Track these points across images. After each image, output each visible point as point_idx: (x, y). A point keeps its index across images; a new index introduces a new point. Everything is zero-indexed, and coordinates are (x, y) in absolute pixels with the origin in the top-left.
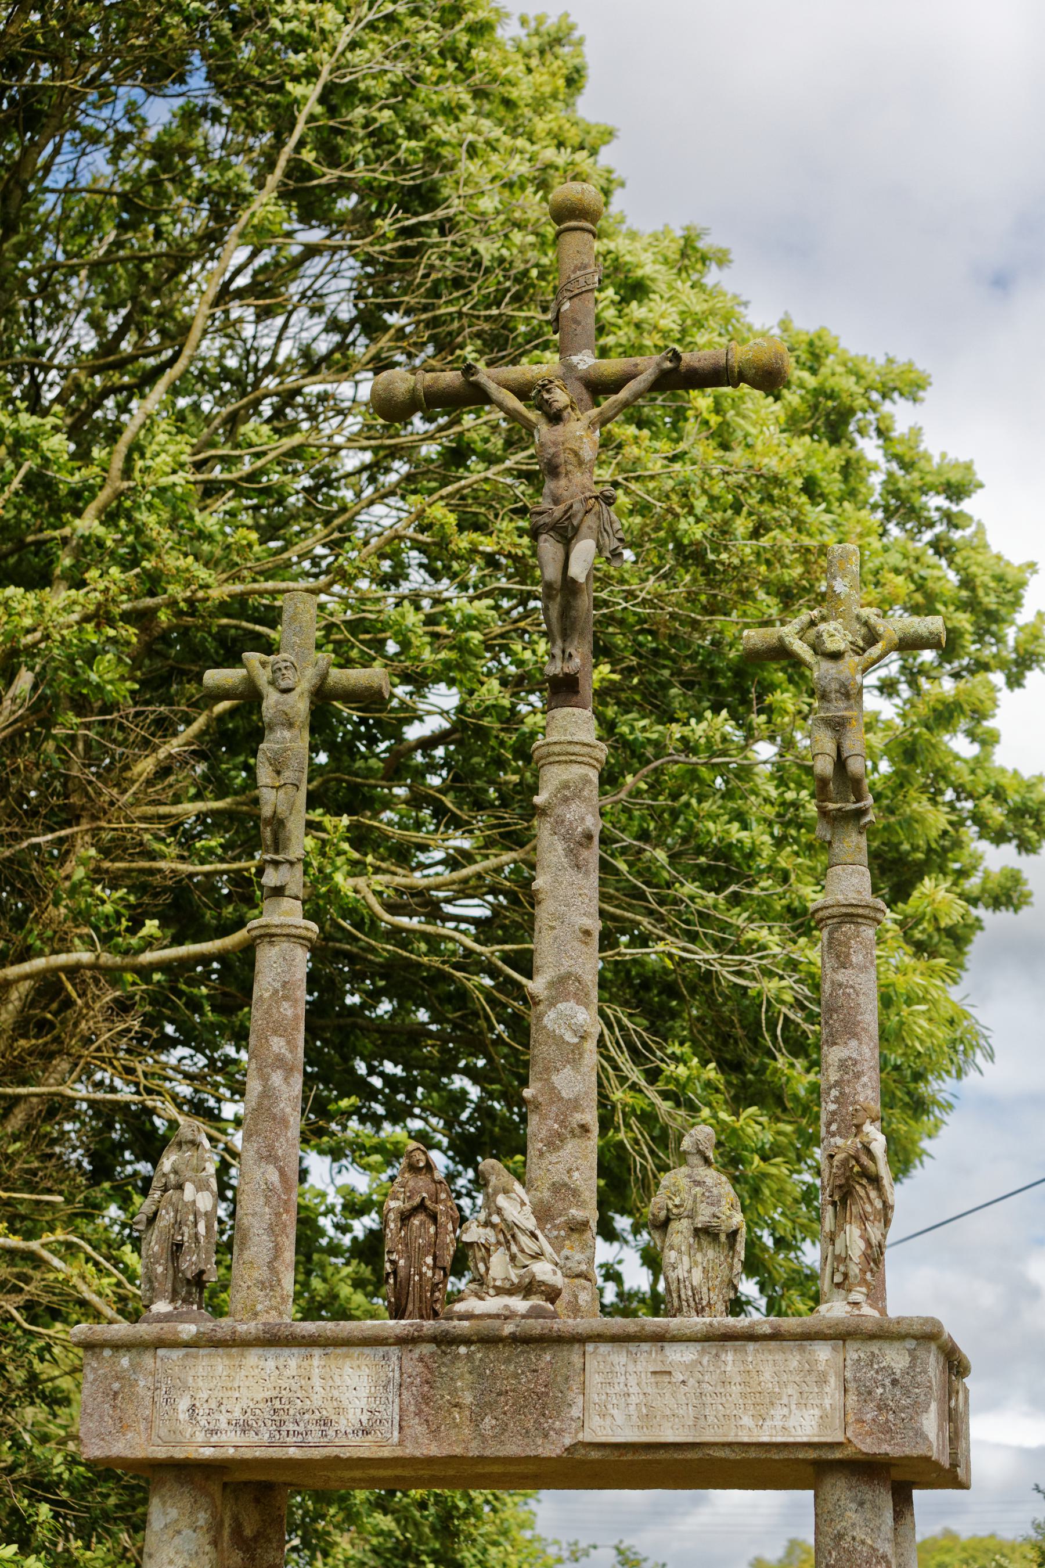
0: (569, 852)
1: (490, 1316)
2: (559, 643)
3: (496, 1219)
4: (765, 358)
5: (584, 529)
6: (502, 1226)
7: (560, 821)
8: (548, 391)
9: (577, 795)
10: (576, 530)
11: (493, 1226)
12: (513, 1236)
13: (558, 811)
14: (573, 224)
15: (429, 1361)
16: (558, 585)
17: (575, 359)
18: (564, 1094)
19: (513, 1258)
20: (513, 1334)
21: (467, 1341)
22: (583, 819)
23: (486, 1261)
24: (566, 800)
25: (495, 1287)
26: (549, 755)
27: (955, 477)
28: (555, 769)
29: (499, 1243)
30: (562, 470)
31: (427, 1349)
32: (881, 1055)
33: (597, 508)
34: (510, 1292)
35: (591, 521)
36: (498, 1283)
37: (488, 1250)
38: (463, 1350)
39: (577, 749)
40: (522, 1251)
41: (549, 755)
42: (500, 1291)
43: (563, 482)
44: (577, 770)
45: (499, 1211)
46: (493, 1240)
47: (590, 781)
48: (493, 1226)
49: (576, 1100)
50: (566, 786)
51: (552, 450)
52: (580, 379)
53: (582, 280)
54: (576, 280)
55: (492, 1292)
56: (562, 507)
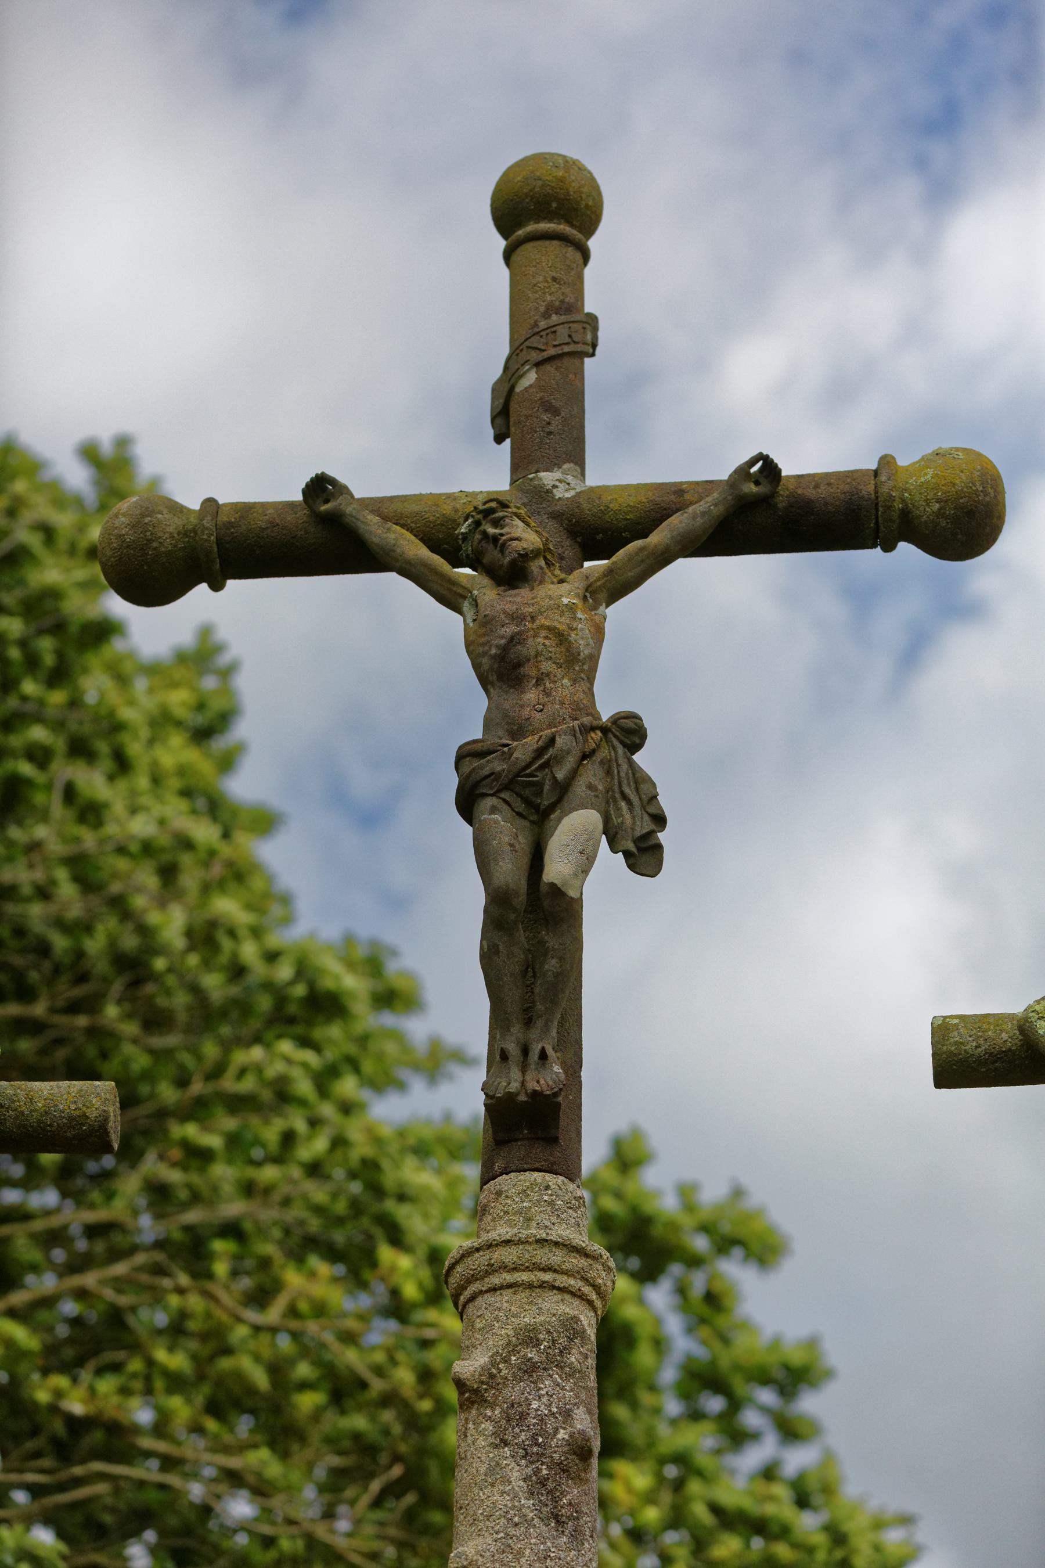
0: (537, 1485)
2: (516, 1030)
4: (961, 480)
5: (579, 788)
7: (516, 1415)
8: (497, 523)
9: (556, 1361)
10: (563, 789)
13: (514, 1392)
14: (544, 226)
16: (520, 901)
17: (547, 478)
22: (567, 1415)
24: (529, 1369)
26: (491, 1270)
27: (797, 1358)
28: (504, 1300)
30: (529, 670)
33: (604, 753)
35: (591, 774)
39: (556, 1257)
41: (491, 1270)
43: (531, 695)
44: (554, 1307)
47: (582, 1334)
50: (529, 1337)
51: (510, 630)
52: (556, 516)
53: (562, 331)
54: (552, 330)
56: (532, 742)
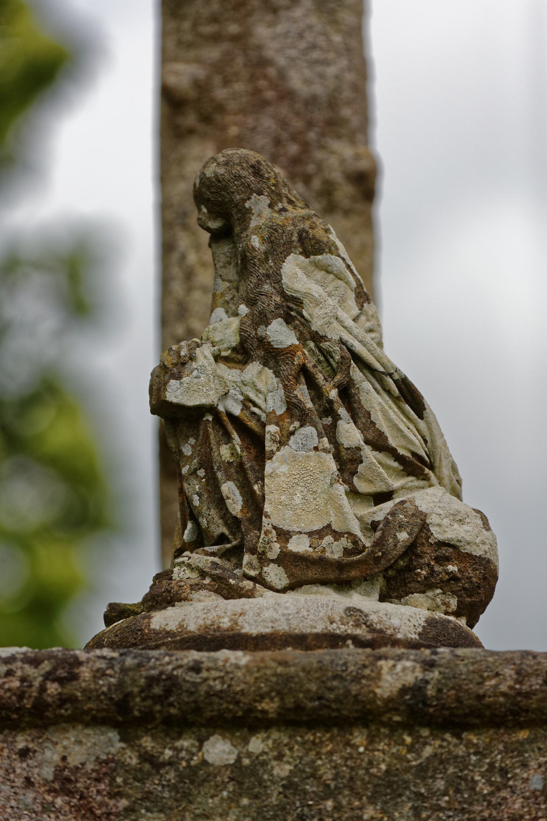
1: (300, 641)
3: (280, 334)
6: (307, 356)
11: (273, 356)
12: (347, 393)
15: (97, 794)
18: (296, 81)
19: (348, 464)
20: (416, 690)
21: (240, 720)
23: (250, 475)
25: (287, 560)
29: (294, 409)
31: (81, 747)
32: (458, 475)
34: (339, 576)
36: (299, 545)
37: (255, 441)
38: (219, 750)
40: (379, 444)
42: (304, 572)
45: (291, 309)
46: (273, 402)
48: (273, 356)
49: (333, 103)
55: (275, 574)
